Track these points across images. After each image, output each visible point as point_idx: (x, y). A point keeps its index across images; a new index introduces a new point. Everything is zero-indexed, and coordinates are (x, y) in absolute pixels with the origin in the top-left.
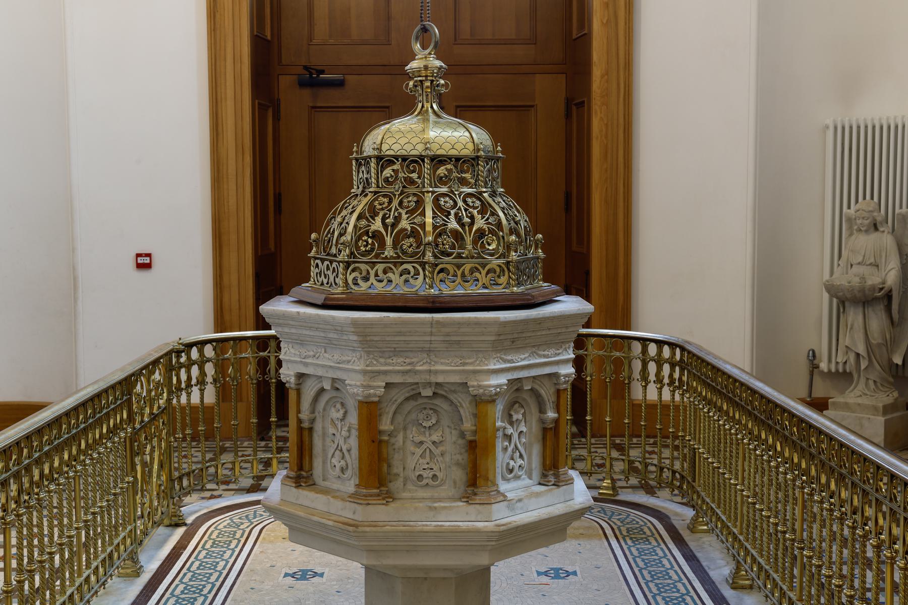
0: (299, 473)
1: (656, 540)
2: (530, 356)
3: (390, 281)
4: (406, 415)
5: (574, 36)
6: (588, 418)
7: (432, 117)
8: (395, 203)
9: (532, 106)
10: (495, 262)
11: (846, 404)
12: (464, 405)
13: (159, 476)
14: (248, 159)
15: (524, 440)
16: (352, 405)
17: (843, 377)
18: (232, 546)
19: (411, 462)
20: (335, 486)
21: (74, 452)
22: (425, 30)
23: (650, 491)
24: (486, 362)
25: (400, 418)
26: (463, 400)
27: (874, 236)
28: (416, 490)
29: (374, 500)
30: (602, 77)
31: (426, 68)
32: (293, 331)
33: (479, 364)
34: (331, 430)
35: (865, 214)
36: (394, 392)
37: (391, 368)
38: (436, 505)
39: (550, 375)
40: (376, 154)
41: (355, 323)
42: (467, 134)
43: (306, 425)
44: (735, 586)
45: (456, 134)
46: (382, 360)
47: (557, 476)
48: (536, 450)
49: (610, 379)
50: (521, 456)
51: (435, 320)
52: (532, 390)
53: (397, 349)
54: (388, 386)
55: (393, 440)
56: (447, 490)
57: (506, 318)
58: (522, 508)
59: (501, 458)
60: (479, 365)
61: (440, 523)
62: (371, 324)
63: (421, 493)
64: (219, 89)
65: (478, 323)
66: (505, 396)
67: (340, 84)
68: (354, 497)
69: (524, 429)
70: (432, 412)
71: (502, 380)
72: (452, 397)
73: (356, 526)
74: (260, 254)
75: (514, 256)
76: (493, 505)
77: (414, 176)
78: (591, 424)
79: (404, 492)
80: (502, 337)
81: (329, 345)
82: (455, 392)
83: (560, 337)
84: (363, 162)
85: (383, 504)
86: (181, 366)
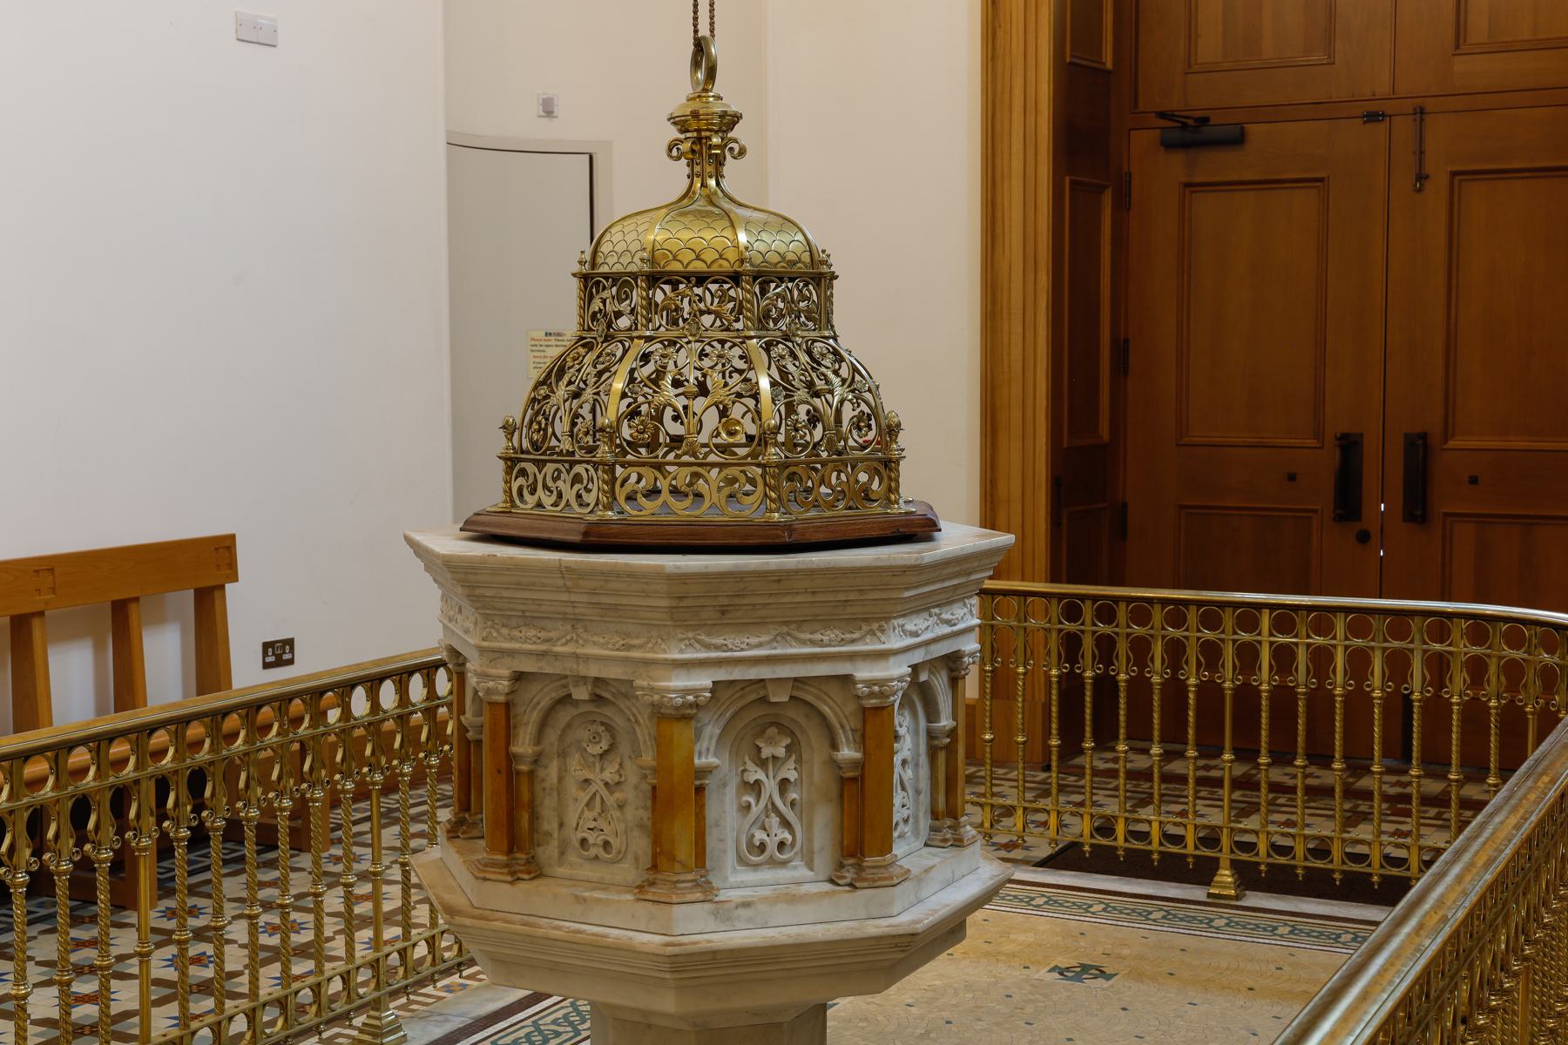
0: (461, 815)
2: (774, 640)
3: (699, 495)
4: (564, 731)
12: (641, 721)
14: (1044, 280)
24: (663, 646)
25: (552, 736)
26: (639, 712)
28: (581, 865)
29: (494, 873)
33: (652, 648)
37: (517, 646)
38: (587, 894)
40: (646, 269)
43: (470, 735)
46: (505, 631)
47: (859, 868)
49: (1534, 707)
51: (564, 565)
53: (527, 614)
54: (519, 677)
57: (679, 567)
58: (750, 920)
60: (652, 650)
61: (577, 926)
63: (588, 872)
64: (998, 161)
65: (631, 575)
66: (727, 709)
69: (792, 776)
70: (603, 728)
74: (1065, 445)
76: (676, 908)
79: (560, 866)
80: (685, 603)
83: (849, 610)
85: (508, 882)
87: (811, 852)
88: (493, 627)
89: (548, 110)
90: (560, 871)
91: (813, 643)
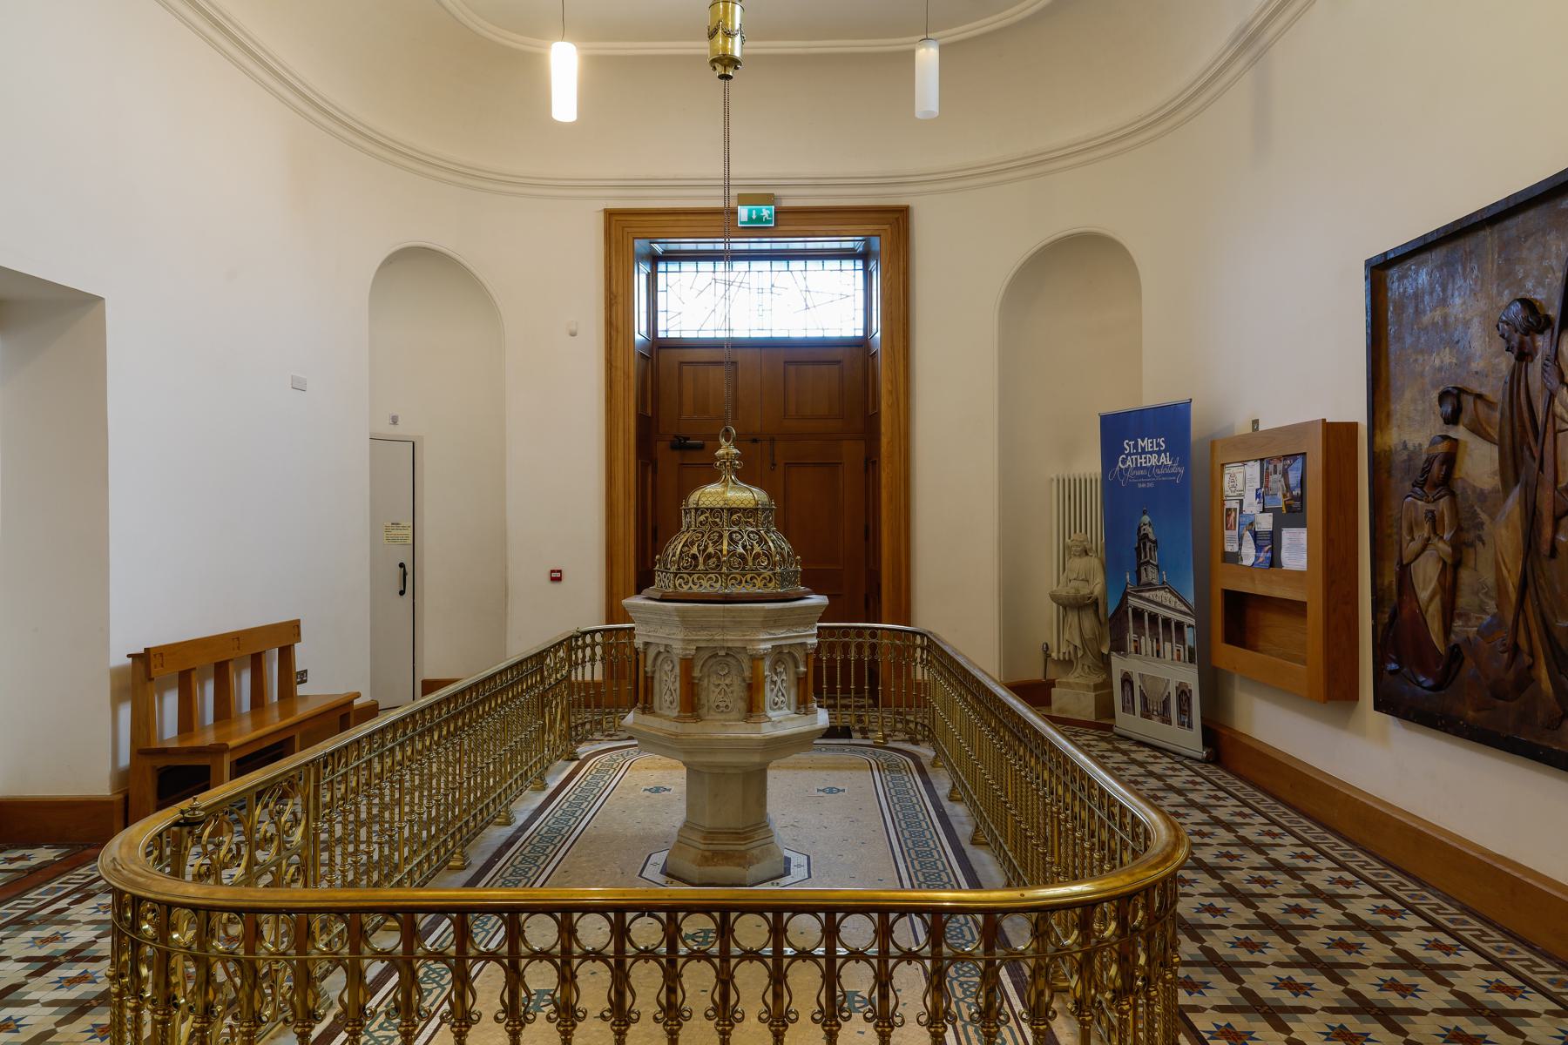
1: (906, 772)
5: (871, 414)
6: (880, 688)
7: (731, 484)
8: (706, 537)
9: (841, 463)
10: (767, 573)
11: (1068, 683)
13: (560, 724)
14: (633, 502)
15: (784, 685)
16: (677, 661)
17: (1067, 664)
18: (610, 772)
19: (712, 697)
20: (667, 713)
21: (504, 699)
22: (727, 430)
23: (915, 742)
25: (705, 670)
27: (1086, 559)
30: (888, 443)
31: (727, 454)
32: (642, 615)
34: (665, 678)
35: (1077, 543)
36: (702, 652)
39: (801, 644)
41: (677, 610)
42: (751, 494)
43: (649, 675)
44: (951, 799)
45: (744, 495)
47: (806, 708)
48: (793, 691)
50: (783, 695)
52: (789, 652)
54: (698, 648)
55: (701, 683)
56: (735, 715)
59: (769, 695)
62: (687, 610)
65: (752, 610)
67: (701, 447)
68: (677, 719)
69: (785, 678)
71: (768, 645)
72: (738, 656)
73: (677, 736)
75: (778, 570)
77: (718, 520)
78: (882, 693)
81: (663, 623)
82: (739, 653)
84: (688, 511)
86: (579, 647)
87: (789, 704)
89: (395, 421)
90: (709, 717)
91: (796, 632)
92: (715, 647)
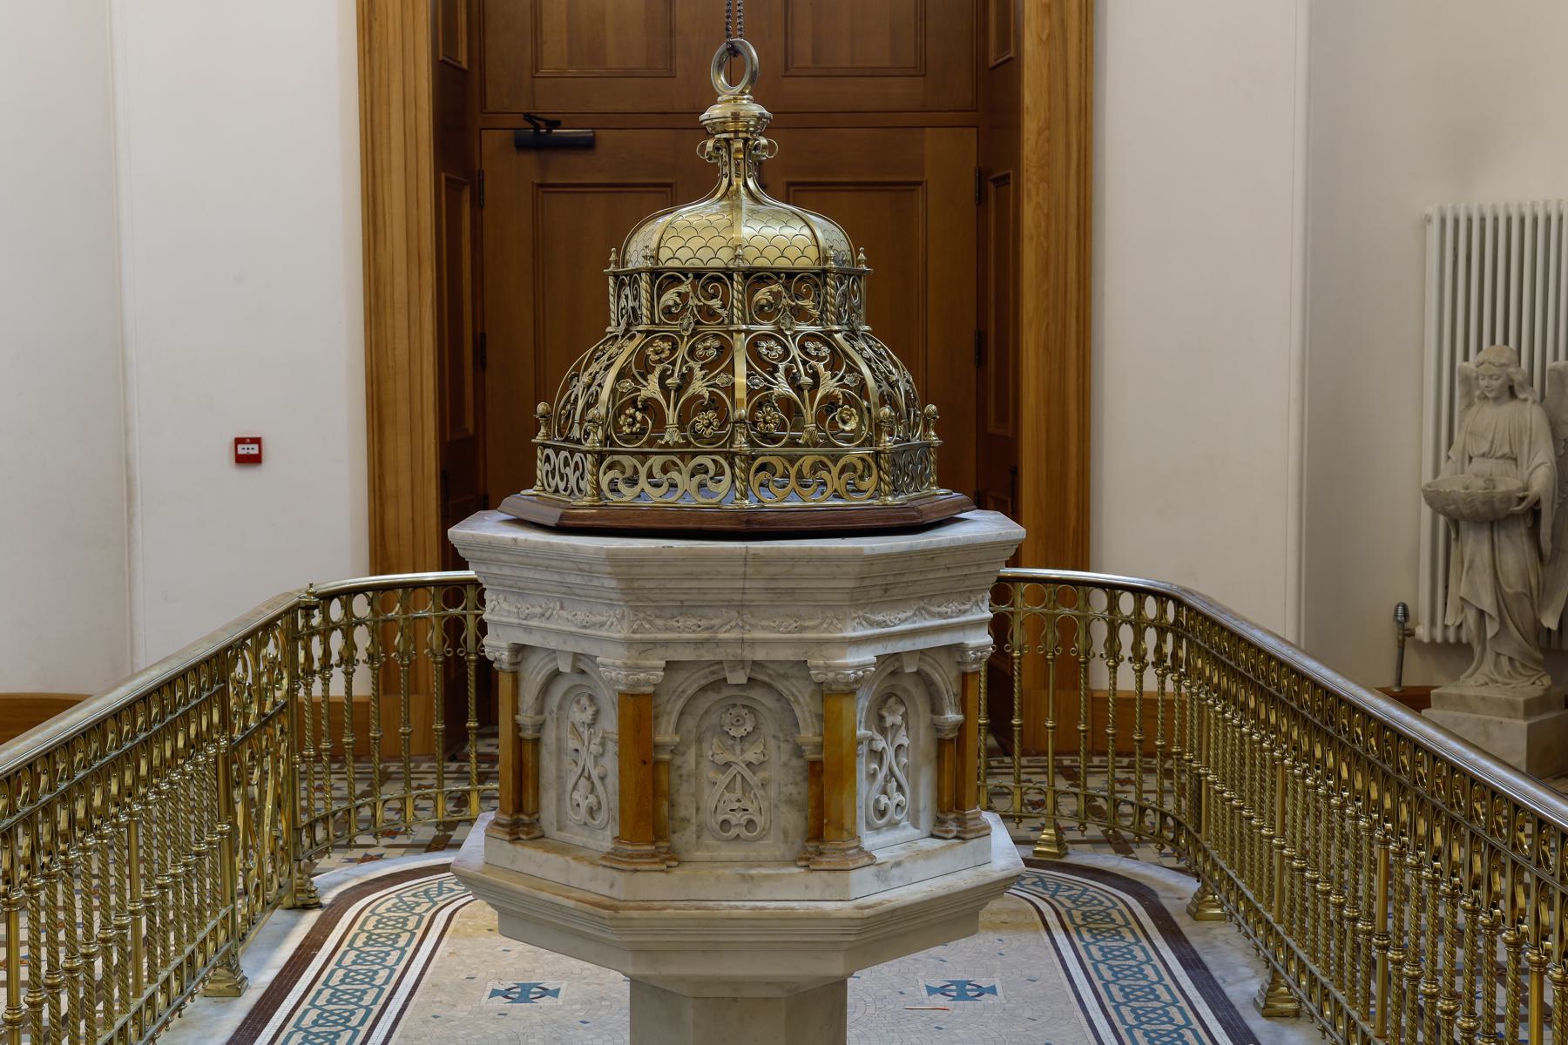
0: (516, 817)
1: (1133, 932)
2: (914, 614)
3: (673, 486)
4: (702, 717)
5: (992, 63)
6: (1016, 722)
7: (746, 202)
8: (683, 350)
9: (919, 184)
10: (855, 453)
11: (1462, 697)
12: (802, 700)
13: (274, 823)
14: (429, 275)
15: (904, 760)
16: (608, 700)
18: (401, 943)
19: (710, 799)
20: (579, 840)
21: (128, 780)
22: (733, 51)
24: (840, 626)
25: (690, 723)
26: (799, 691)
27: (1510, 407)
28: (719, 847)
29: (646, 863)
30: (1040, 132)
31: (736, 117)
32: (507, 571)
33: (827, 628)
34: (572, 743)
35: (1494, 370)
36: (680, 677)
37: (674, 636)
38: (753, 872)
39: (949, 648)
40: (650, 265)
41: (613, 557)
42: (806, 231)
43: (528, 734)
44: (1268, 1013)
45: (788, 231)
46: (659, 622)
47: (961, 822)
48: (926, 777)
49: (1054, 654)
50: (900, 788)
51: (751, 552)
52: (919, 673)
53: (686, 604)
54: (670, 666)
55: (678, 761)
56: (771, 847)
57: (873, 549)
58: (901, 878)
59: (866, 792)
60: (827, 630)
61: (760, 904)
62: (640, 559)
63: (727, 852)
64: (378, 154)
65: (825, 558)
66: (873, 684)
68: (612, 859)
69: (905, 741)
70: (746, 711)
71: (867, 656)
72: (780, 685)
73: (615, 909)
74: (448, 439)
75: (887, 442)
76: (852, 873)
77: (716, 303)
78: (1021, 733)
79: (698, 850)
81: (568, 595)
82: (785, 676)
83: (967, 583)
84: (627, 279)
85: (662, 871)
86: (313, 632)
88: (644, 619)
92: (721, 662)
